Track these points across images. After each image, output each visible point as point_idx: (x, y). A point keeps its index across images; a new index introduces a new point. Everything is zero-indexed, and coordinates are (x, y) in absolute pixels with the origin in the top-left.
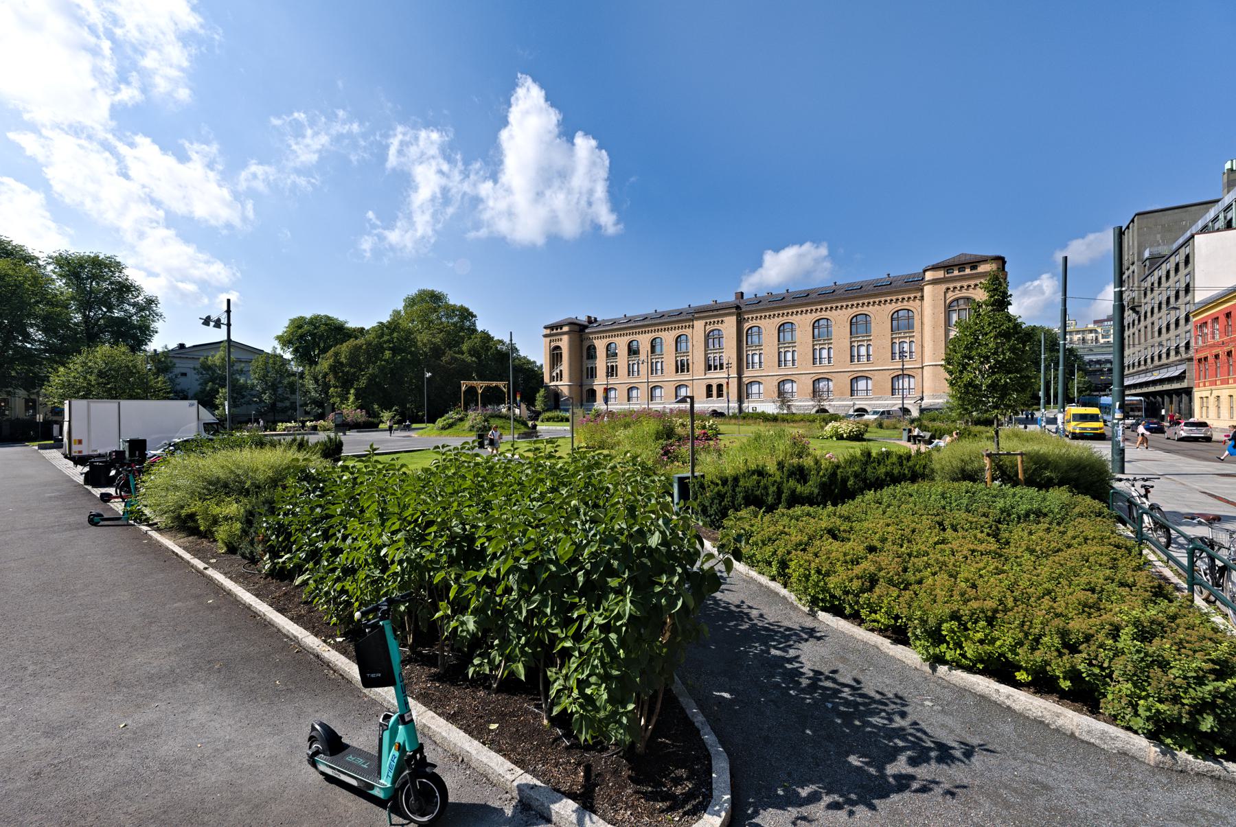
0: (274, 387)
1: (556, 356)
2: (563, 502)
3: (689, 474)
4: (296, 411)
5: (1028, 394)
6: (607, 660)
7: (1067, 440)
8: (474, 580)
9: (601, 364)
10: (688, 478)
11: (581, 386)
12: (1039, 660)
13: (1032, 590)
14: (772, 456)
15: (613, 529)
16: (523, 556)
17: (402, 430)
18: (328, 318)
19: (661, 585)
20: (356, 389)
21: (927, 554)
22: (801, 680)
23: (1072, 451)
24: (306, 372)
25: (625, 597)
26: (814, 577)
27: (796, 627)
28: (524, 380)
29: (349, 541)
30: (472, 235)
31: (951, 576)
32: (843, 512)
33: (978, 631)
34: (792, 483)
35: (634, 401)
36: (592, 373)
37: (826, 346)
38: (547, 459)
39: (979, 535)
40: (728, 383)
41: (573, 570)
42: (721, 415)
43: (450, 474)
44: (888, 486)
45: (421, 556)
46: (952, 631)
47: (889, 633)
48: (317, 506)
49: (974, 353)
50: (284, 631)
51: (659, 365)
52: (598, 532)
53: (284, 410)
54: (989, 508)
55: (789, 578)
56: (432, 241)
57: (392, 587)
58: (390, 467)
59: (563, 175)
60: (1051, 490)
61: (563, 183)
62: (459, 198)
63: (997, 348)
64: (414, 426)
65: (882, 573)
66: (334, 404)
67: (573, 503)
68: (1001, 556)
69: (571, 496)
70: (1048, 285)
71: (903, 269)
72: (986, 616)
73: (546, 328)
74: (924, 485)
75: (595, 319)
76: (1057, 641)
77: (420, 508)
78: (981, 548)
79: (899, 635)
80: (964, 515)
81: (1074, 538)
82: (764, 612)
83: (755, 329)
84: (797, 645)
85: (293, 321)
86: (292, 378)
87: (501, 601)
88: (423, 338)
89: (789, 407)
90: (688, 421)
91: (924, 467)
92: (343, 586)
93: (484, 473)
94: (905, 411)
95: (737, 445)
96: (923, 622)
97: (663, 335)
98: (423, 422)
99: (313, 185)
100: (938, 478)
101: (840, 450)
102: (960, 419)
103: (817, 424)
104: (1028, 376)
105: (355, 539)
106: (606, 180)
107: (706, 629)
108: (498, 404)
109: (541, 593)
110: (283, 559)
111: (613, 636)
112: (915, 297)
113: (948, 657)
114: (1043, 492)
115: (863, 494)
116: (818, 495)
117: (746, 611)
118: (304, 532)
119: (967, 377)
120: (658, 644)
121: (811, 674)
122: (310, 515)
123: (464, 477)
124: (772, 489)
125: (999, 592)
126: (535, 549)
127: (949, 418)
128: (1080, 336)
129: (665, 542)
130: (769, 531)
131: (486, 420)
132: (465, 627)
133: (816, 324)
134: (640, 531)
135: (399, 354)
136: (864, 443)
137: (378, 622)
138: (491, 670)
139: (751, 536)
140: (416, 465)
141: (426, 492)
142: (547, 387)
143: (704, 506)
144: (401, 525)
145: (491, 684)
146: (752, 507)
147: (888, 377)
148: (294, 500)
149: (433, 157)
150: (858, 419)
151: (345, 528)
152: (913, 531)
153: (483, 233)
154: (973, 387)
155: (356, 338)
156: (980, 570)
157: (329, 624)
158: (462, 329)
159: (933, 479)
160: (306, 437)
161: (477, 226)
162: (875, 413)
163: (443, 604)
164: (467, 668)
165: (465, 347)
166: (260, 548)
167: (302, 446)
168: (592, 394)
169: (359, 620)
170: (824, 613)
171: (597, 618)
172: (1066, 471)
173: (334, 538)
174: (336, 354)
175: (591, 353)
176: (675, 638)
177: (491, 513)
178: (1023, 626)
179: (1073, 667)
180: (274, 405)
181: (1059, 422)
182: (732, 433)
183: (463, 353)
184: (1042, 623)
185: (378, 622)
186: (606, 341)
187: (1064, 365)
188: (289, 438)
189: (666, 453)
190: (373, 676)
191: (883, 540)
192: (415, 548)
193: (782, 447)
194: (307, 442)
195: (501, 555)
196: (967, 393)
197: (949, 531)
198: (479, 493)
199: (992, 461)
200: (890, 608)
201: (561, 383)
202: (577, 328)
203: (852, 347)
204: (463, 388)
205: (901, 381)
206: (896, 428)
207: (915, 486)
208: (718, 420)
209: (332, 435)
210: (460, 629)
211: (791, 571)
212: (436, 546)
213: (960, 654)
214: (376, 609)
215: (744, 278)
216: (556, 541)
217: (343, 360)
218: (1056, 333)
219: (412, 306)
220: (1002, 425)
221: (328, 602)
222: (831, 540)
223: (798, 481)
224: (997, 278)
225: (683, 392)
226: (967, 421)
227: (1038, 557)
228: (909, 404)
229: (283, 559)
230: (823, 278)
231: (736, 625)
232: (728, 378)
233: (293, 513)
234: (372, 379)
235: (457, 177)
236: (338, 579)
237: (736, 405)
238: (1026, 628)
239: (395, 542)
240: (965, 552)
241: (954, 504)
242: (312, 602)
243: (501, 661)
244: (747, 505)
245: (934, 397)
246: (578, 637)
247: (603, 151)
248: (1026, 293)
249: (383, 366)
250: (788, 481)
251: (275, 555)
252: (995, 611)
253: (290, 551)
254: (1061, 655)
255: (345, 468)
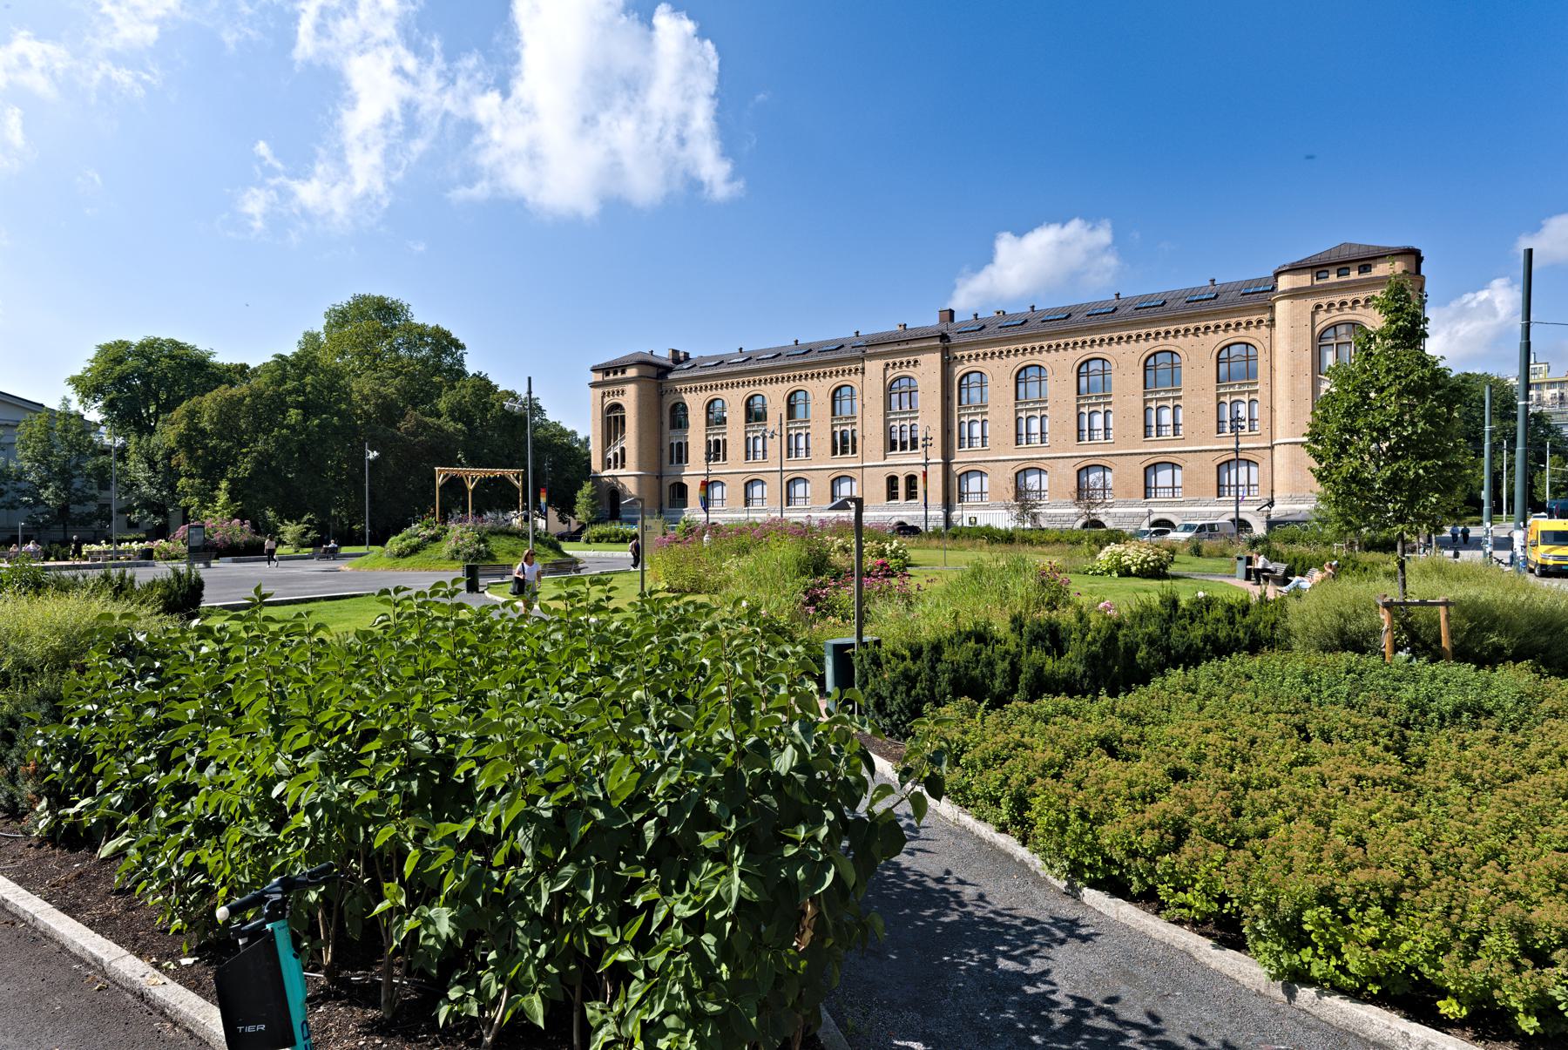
0: (65, 475)
1: (613, 422)
2: (617, 694)
3: (854, 640)
4: (109, 520)
5: (1459, 493)
6: (698, 984)
7: (1531, 578)
8: (451, 839)
9: (696, 437)
10: (852, 646)
11: (660, 477)
12: (1480, 978)
13: (1465, 849)
14: (1003, 605)
15: (709, 743)
16: (544, 792)
17: (321, 558)
18: (176, 345)
19: (795, 843)
20: (231, 481)
21: (1276, 783)
22: (1052, 1016)
23: (1537, 598)
24: (132, 448)
25: (730, 866)
26: (1075, 826)
27: (1043, 917)
28: (554, 465)
29: (211, 770)
30: (460, 194)
31: (1319, 823)
32: (1127, 707)
33: (1368, 925)
34: (1037, 655)
35: (757, 504)
36: (680, 454)
37: (1170, 404)
38: (592, 613)
39: (1370, 750)
40: (925, 474)
41: (636, 817)
42: (914, 531)
43: (409, 641)
44: (1209, 659)
45: (352, 798)
46: (1322, 924)
47: (1209, 928)
48: (149, 705)
49: (1360, 423)
50: (74, 950)
51: (802, 440)
52: (683, 748)
53: (85, 520)
54: (1388, 699)
55: (1032, 827)
56: (385, 203)
57: (294, 858)
58: (296, 628)
59: (633, 85)
60: (1500, 669)
61: (632, 100)
62: (436, 123)
63: (1402, 414)
64: (345, 550)
65: (1196, 819)
66: (186, 509)
67: (636, 694)
68: (1409, 787)
69: (631, 681)
70: (1503, 297)
71: (1235, 272)
72: (1382, 898)
73: (595, 370)
74: (1270, 659)
75: (687, 355)
76: (1511, 943)
77: (350, 706)
78: (1374, 772)
79: (1228, 933)
80: (1344, 713)
81: (1541, 755)
82: (986, 889)
83: (973, 377)
84: (1045, 951)
85: (104, 350)
86: (102, 459)
87: (502, 878)
88: (361, 385)
89: (1034, 517)
90: (853, 543)
91: (1273, 627)
92: (197, 858)
93: (473, 639)
94: (1242, 525)
95: (939, 585)
96: (1270, 907)
97: (810, 385)
98: (362, 543)
99: (145, 84)
100: (1297, 646)
101: (1124, 595)
102: (1339, 539)
103: (1084, 549)
104: (1457, 465)
105: (222, 767)
106: (713, 97)
107: (879, 923)
108: (506, 510)
109: (577, 862)
110: (77, 808)
111: (708, 939)
112: (1260, 322)
113: (1315, 973)
114: (1485, 672)
115: (1163, 675)
116: (1084, 675)
117: (954, 888)
118: (119, 754)
119: (1348, 465)
120: (791, 952)
121: (1070, 1005)
122: (134, 722)
123: (435, 648)
124: (1002, 666)
125: (1406, 854)
126: (566, 781)
127: (1319, 535)
128: (1556, 391)
129: (803, 766)
130: (995, 741)
131: (482, 540)
132: (432, 930)
133: (1083, 369)
134: (759, 746)
135: (316, 416)
136: (1167, 583)
137: (263, 924)
138: (481, 1010)
139: (963, 752)
140: (344, 625)
141: (362, 676)
142: (597, 479)
143: (880, 697)
144: (313, 738)
145: (481, 1036)
146: (966, 699)
147: (1211, 463)
148: (100, 694)
149: (386, 43)
150: (1156, 540)
151: (204, 745)
152: (1253, 742)
153: (481, 190)
154: (1358, 483)
155: (232, 384)
156: (1371, 813)
157: (167, 931)
158: (437, 369)
159: (1289, 648)
160: (129, 572)
161: (471, 176)
162: (1188, 528)
163: (391, 887)
164: (435, 1006)
165: (442, 404)
166: (28, 788)
167: (122, 589)
168: (680, 491)
169: (228, 922)
170: (1093, 892)
171: (678, 906)
172: (1527, 635)
173: (182, 765)
174: (192, 414)
175: (679, 416)
176: (823, 941)
177: (486, 713)
178: (1448, 915)
179: (1542, 992)
180: (64, 510)
181: (1517, 545)
182: (932, 565)
183: (439, 416)
184: (1483, 910)
185: (263, 924)
186: (705, 396)
187: (1526, 444)
188: (95, 574)
189: (813, 601)
190: (250, 1029)
191: (1199, 758)
192: (340, 781)
193: (1020, 590)
194: (132, 581)
195: (503, 792)
196: (1350, 493)
197: (1317, 741)
198: (465, 675)
199: (1394, 615)
200: (1211, 882)
201: (623, 472)
202: (652, 372)
203: (1146, 410)
204: (439, 481)
205: (1233, 472)
206: (1224, 555)
207: (1257, 661)
208: (907, 541)
209: (183, 567)
210: (423, 933)
211: (1034, 815)
212: (380, 777)
213: (1337, 967)
214: (260, 900)
215: (959, 281)
216: (606, 765)
217: (206, 425)
218: (1512, 387)
219: (342, 326)
220: (1413, 550)
221: (166, 889)
222: (1105, 758)
223: (1048, 652)
224: (1402, 289)
225: (845, 490)
226: (1352, 544)
227: (1476, 790)
228: (1248, 512)
229: (77, 808)
230: (1098, 288)
231: (935, 916)
232: (926, 465)
233: (99, 719)
234: (263, 461)
235: (432, 82)
236: (188, 844)
237: (941, 514)
238: (1454, 918)
239: (301, 770)
240: (1344, 780)
241: (1326, 694)
242: (133, 889)
243: (500, 992)
244: (956, 696)
245: (1292, 499)
246: (643, 943)
247: (708, 43)
248: (1464, 313)
249: (286, 438)
250: (1029, 652)
251: (59, 799)
252: (1399, 888)
253: (91, 792)
254: (1518, 969)
255: (205, 632)
